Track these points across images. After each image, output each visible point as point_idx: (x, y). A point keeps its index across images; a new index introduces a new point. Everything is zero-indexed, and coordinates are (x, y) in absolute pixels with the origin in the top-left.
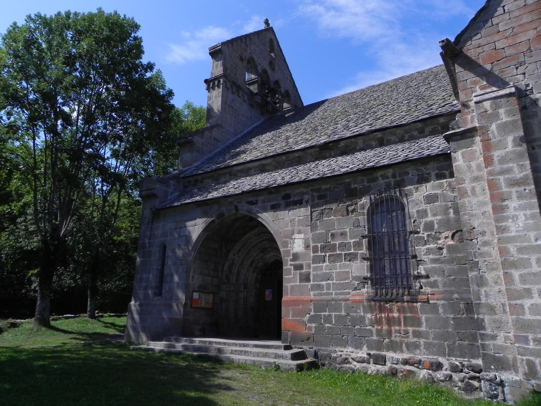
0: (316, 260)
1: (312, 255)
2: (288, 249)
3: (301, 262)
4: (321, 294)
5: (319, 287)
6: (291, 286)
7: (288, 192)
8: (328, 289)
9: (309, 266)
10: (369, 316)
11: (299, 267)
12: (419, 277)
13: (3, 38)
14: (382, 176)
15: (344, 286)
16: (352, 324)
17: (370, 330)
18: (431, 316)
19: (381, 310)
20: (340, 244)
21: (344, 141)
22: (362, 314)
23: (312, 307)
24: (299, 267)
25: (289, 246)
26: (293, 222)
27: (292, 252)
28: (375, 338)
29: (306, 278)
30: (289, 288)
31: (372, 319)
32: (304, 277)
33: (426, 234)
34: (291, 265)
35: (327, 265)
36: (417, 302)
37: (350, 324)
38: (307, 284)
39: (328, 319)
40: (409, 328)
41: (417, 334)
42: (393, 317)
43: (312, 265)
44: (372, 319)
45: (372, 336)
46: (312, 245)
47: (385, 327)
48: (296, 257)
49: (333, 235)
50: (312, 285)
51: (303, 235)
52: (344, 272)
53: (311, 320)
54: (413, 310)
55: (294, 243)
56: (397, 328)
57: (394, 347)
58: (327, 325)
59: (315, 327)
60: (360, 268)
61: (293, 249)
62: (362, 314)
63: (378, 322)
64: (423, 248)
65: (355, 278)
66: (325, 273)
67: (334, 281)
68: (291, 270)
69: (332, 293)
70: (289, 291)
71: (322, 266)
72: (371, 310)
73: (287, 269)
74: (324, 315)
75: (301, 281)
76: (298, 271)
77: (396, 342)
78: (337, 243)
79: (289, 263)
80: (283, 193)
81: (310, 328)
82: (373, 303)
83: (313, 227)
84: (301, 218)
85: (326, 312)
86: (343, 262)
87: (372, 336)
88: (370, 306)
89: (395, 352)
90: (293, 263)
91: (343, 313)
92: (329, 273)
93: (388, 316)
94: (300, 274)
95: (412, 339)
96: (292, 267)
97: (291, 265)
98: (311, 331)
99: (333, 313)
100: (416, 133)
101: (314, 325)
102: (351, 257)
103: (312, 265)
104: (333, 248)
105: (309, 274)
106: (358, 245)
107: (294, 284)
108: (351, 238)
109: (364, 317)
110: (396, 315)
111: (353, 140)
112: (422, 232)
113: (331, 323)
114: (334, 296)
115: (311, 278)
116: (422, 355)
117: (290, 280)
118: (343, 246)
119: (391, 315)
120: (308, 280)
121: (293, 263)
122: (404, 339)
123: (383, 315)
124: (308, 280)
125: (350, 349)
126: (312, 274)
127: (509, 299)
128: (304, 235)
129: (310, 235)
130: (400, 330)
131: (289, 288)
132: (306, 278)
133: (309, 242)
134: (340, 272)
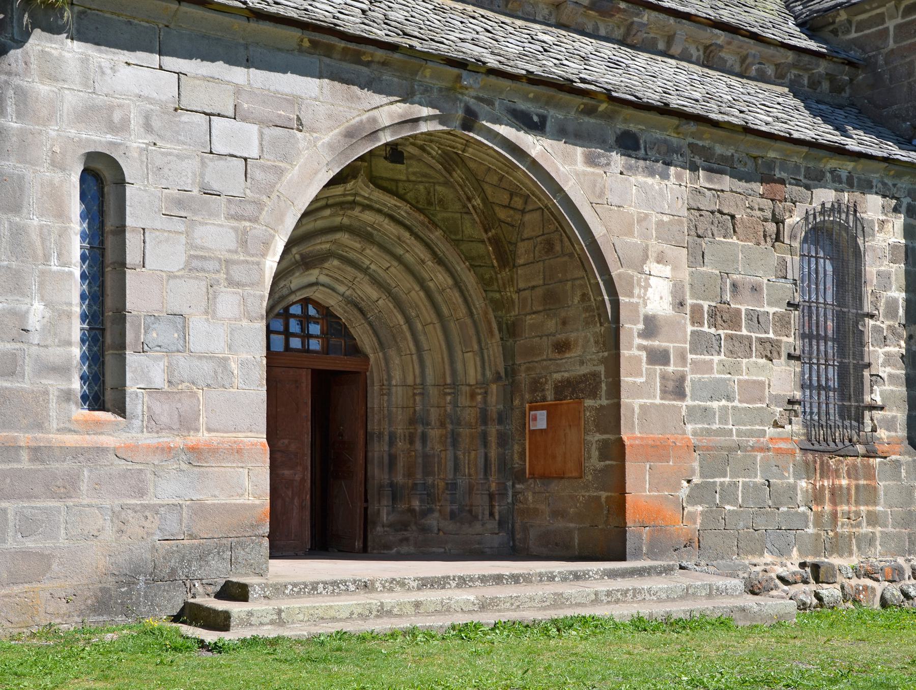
0: (700, 343)
1: (690, 328)
2: (635, 300)
3: (664, 344)
4: (709, 432)
5: (706, 414)
6: (641, 406)
7: (632, 127)
8: (723, 420)
9: (683, 358)
10: (803, 484)
11: (659, 357)
12: (873, 408)
13: (199, 648)
14: (832, 172)
15: (759, 416)
16: (774, 503)
17: (804, 514)
18: (892, 483)
19: (825, 472)
20: (748, 313)
21: (654, 14)
22: (792, 480)
23: (696, 465)
24: (659, 357)
25: (636, 291)
26: (644, 224)
27: (642, 311)
28: (811, 530)
29: (677, 389)
30: (637, 410)
31: (807, 491)
32: (671, 385)
33: (887, 323)
34: (641, 348)
35: (720, 361)
36: (875, 457)
37: (770, 503)
38: (678, 403)
39: (728, 493)
40: (862, 508)
41: (873, 519)
42: (841, 486)
43: (690, 356)
44: (807, 491)
45: (807, 527)
46: (689, 301)
47: (828, 508)
48: (651, 327)
49: (734, 286)
50: (690, 409)
51: (669, 268)
52: (754, 382)
53: (693, 499)
54: (869, 473)
55: (648, 286)
56: (846, 508)
57: (839, 546)
58: (728, 507)
59: (702, 513)
60: (782, 378)
61: (645, 305)
62: (792, 480)
63: (817, 497)
64: (880, 350)
65: (776, 399)
66: (718, 381)
67: (736, 403)
68: (640, 360)
69: (731, 430)
70: (636, 421)
71: (712, 360)
72: (807, 470)
73: (630, 357)
74: (722, 484)
75: (665, 393)
76: (658, 368)
77: (842, 536)
78: (743, 308)
79: (638, 341)
80: (621, 126)
81: (692, 517)
82: (810, 457)
83: (698, 257)
84: (666, 218)
85: (725, 476)
86: (754, 359)
87: (807, 527)
88: (807, 463)
89: (841, 556)
90: (645, 343)
91: (759, 480)
92: (725, 380)
93: (833, 484)
94: (664, 377)
95: (865, 529)
96: (644, 355)
97: (641, 348)
98: (695, 523)
99: (741, 480)
100: (770, 71)
101: (700, 508)
102: (770, 351)
103: (690, 356)
104: (733, 320)
105: (682, 379)
106: (782, 323)
107: (649, 401)
108: (770, 304)
109: (794, 488)
110: (844, 482)
111: (672, 20)
112: (881, 319)
113: (734, 502)
114: (735, 438)
115: (688, 391)
116: (878, 557)
117: (639, 391)
118: (757, 320)
119: (837, 482)
120: (680, 393)
121: (645, 343)
122: (854, 530)
123: (826, 484)
124: (680, 393)
125: (768, 558)
126: (689, 378)
127: (486, 232)
128: (673, 269)
129: (685, 274)
130: (849, 512)
131: (637, 410)
132: (677, 389)
133: (683, 293)
134: (747, 381)
